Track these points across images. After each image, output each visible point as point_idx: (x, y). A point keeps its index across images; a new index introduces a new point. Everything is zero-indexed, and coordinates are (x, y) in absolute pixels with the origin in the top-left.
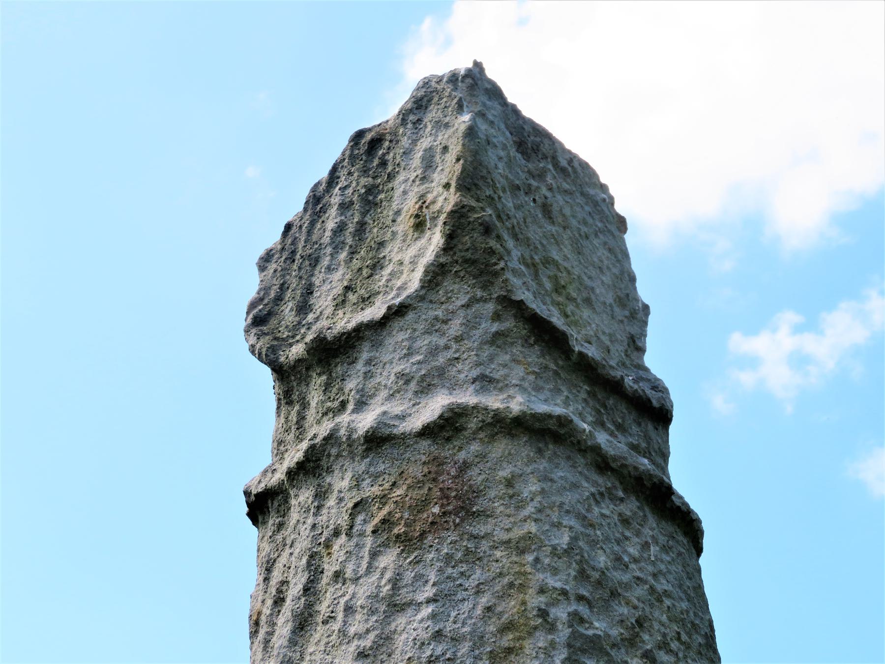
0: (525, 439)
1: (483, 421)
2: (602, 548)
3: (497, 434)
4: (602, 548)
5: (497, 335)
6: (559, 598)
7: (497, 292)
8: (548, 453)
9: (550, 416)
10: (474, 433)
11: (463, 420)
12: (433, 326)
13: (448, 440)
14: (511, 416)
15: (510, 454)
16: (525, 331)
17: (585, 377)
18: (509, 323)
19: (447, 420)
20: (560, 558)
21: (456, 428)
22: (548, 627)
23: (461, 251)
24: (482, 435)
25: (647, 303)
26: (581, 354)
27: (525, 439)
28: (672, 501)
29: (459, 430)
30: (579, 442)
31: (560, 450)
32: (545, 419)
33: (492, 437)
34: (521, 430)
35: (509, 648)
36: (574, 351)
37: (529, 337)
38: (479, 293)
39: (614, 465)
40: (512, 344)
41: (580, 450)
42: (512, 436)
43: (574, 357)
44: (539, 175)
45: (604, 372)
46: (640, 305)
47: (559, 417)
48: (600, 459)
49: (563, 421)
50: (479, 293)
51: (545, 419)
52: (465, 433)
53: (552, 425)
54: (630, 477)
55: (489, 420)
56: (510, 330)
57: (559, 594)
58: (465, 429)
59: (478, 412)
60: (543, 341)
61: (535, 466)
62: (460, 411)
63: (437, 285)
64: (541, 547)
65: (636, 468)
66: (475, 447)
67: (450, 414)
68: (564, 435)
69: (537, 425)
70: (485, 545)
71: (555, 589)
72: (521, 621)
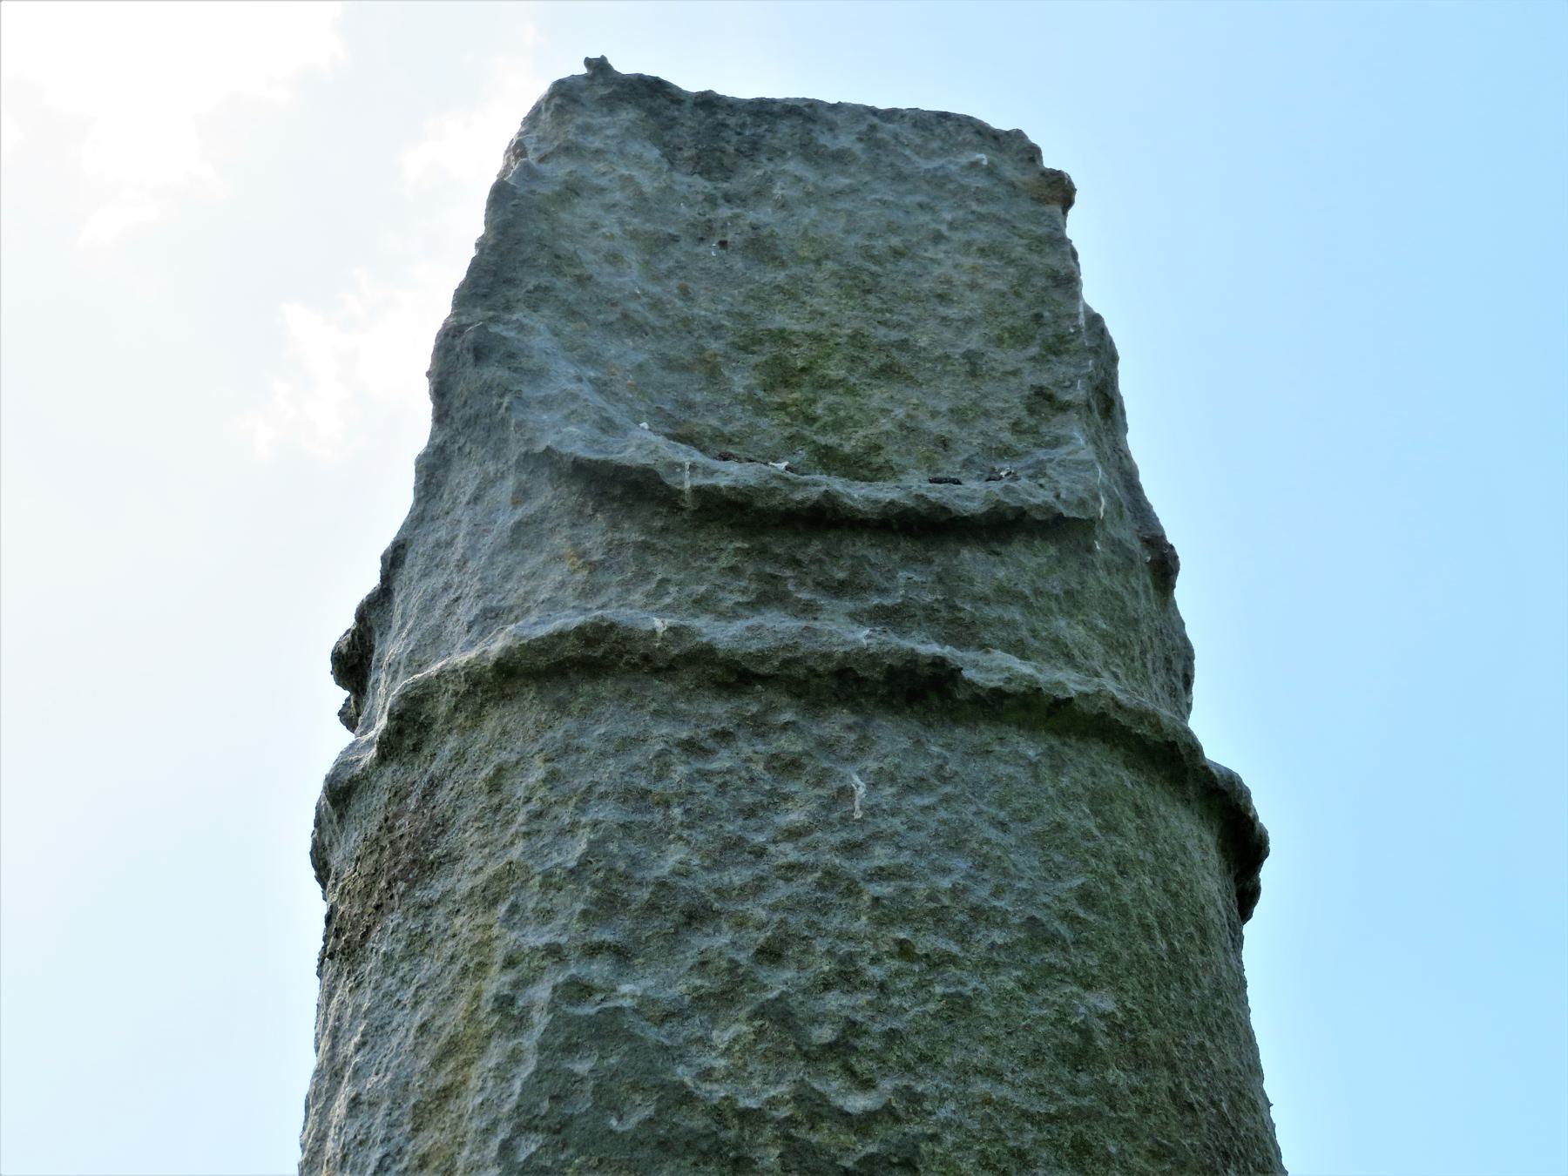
0: (532, 694)
1: (456, 694)
2: (680, 838)
3: (482, 706)
4: (680, 838)
5: (519, 527)
6: (545, 963)
7: (515, 451)
8: (575, 708)
9: (562, 635)
10: (448, 721)
11: (428, 705)
12: (432, 559)
13: (416, 748)
14: (489, 665)
15: (504, 733)
16: (574, 498)
17: (731, 526)
18: (545, 495)
19: (400, 717)
20: (560, 890)
21: (422, 725)
22: (512, 1025)
23: (458, 410)
24: (460, 718)
25: (1096, 310)
26: (697, 491)
27: (532, 694)
28: (970, 684)
29: (425, 727)
30: (646, 658)
31: (606, 688)
32: (554, 645)
33: (478, 717)
34: (520, 682)
35: (445, 1089)
36: (681, 492)
37: (584, 505)
38: (491, 468)
39: (764, 669)
40: (552, 530)
41: (656, 671)
42: (505, 698)
43: (689, 504)
44: (757, 193)
45: (776, 501)
46: (1082, 321)
47: (580, 631)
48: (718, 671)
49: (592, 635)
50: (491, 468)
51: (554, 645)
52: (437, 727)
53: (571, 649)
54: (819, 676)
55: (463, 688)
56: (545, 509)
57: (543, 958)
58: (435, 719)
59: (447, 682)
60: (614, 499)
61: (549, 734)
62: (419, 692)
63: (439, 485)
64: (527, 880)
65: (827, 657)
66: (452, 742)
67: (403, 704)
68: (604, 657)
69: (542, 662)
70: (439, 917)
71: (534, 950)
72: (469, 1031)
